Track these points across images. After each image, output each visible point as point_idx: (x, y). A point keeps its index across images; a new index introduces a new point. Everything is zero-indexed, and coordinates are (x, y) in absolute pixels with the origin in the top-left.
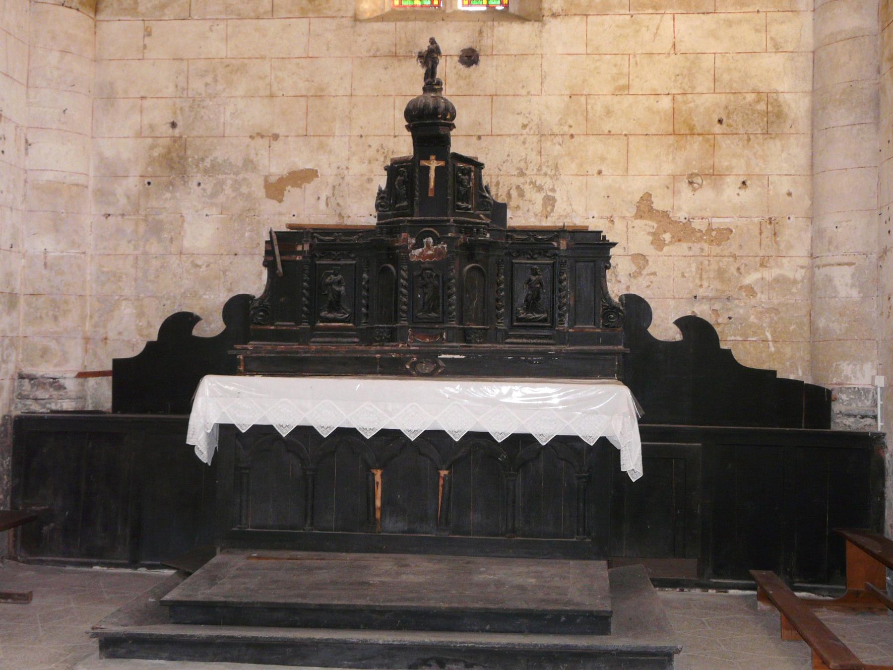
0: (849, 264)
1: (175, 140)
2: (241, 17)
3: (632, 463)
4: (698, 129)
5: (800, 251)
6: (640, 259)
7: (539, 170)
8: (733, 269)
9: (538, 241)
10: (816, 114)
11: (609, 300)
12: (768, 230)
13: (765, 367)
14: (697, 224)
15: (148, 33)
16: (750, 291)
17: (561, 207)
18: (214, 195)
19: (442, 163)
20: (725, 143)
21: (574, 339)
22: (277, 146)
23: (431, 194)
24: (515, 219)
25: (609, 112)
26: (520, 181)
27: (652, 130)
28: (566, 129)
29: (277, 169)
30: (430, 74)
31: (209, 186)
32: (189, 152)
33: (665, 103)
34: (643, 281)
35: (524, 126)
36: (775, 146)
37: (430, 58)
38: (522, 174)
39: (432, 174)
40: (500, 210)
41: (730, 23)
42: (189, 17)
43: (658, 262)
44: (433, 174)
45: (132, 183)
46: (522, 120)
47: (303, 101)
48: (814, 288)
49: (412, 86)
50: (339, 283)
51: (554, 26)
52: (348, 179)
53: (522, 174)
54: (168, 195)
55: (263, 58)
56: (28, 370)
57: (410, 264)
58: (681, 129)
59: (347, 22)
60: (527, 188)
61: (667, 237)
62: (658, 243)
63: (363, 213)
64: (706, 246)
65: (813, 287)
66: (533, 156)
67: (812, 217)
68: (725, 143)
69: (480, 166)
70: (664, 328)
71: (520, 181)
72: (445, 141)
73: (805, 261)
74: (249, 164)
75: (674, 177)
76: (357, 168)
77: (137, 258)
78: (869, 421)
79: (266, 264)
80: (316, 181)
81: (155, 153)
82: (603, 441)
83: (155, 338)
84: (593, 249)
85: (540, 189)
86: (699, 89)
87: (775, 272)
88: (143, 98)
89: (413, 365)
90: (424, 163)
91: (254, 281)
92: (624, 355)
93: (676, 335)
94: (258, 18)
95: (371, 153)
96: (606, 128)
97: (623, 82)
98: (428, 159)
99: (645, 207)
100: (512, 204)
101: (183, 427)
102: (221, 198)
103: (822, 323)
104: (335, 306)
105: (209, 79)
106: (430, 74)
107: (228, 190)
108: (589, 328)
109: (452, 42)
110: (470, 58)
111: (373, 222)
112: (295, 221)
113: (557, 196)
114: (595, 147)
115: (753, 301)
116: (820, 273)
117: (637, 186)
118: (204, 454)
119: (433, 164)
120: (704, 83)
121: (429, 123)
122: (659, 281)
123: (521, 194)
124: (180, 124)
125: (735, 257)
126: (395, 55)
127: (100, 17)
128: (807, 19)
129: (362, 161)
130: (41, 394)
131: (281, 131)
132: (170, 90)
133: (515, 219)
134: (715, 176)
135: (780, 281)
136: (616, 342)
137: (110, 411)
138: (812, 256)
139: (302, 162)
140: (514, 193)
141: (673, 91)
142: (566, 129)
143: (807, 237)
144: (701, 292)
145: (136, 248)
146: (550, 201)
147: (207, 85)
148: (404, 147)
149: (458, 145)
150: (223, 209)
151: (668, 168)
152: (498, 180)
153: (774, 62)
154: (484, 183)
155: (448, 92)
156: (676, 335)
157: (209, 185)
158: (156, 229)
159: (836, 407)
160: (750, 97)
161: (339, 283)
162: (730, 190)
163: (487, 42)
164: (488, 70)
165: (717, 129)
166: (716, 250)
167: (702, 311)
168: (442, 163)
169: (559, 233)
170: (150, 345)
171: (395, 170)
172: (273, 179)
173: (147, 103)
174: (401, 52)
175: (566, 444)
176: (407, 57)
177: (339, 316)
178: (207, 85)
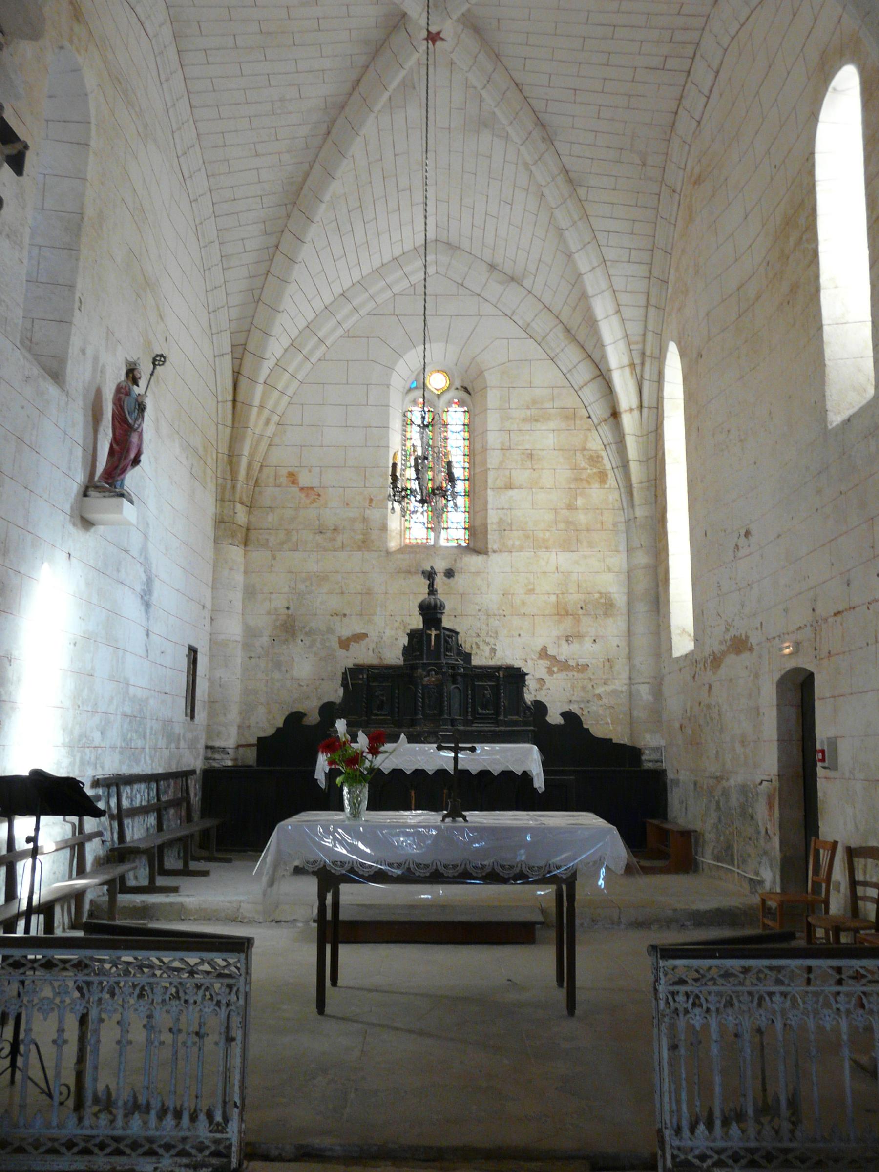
0: (648, 683)
1: (288, 616)
2: (325, 550)
3: (539, 783)
4: (570, 612)
5: (624, 676)
7: (487, 634)
8: (590, 686)
9: (490, 673)
10: (629, 604)
11: (525, 703)
12: (607, 665)
13: (608, 737)
14: (571, 663)
15: (274, 558)
16: (599, 697)
17: (499, 654)
18: (310, 647)
19: (438, 632)
20: (585, 620)
21: (507, 724)
22: (345, 620)
23: (432, 648)
24: (476, 661)
25: (523, 603)
26: (477, 640)
27: (547, 612)
28: (501, 612)
29: (346, 633)
30: (431, 586)
31: (307, 642)
32: (297, 624)
33: (553, 598)
34: (543, 693)
35: (479, 610)
36: (610, 621)
37: (430, 575)
38: (478, 636)
39: (433, 638)
40: (468, 657)
41: (585, 557)
42: (296, 550)
43: (550, 682)
44: (432, 640)
45: (265, 640)
46: (477, 608)
47: (359, 596)
49: (422, 593)
50: (383, 695)
51: (494, 557)
52: (385, 638)
53: (478, 636)
54: (285, 647)
55: (337, 572)
56: (211, 744)
57: (423, 685)
58: (562, 612)
59: (383, 554)
60: (481, 644)
61: (555, 669)
62: (550, 672)
63: (394, 656)
64: (575, 674)
65: (631, 695)
66: (484, 627)
67: (630, 658)
68: (585, 620)
69: (457, 633)
70: (554, 717)
71: (477, 640)
72: (440, 621)
73: (627, 681)
74: (330, 630)
75: (558, 638)
76: (389, 633)
77: (267, 682)
78: (659, 764)
79: (342, 685)
80: (367, 639)
81: (278, 623)
82: (525, 773)
83: (281, 725)
84: (515, 677)
85: (488, 644)
86: (571, 591)
87: (612, 687)
88: (271, 593)
89: (425, 738)
90: (429, 632)
92: (533, 731)
93: (560, 721)
94: (335, 551)
95: (396, 624)
96: (522, 612)
97: (531, 587)
98: (430, 630)
99: (543, 653)
100: (473, 652)
101: (313, 772)
102: (315, 649)
103: (635, 713)
104: (380, 708)
105: (308, 583)
106: (431, 586)
107: (318, 644)
108: (515, 718)
109: (440, 566)
110: (449, 574)
111: (402, 663)
112: (357, 661)
113: (497, 648)
114: (516, 621)
115: (601, 702)
116: (634, 687)
117: (538, 643)
119: (433, 633)
120: (573, 589)
121: (431, 612)
123: (478, 647)
124: (291, 608)
125: (591, 679)
126: (409, 572)
127: (247, 549)
128: (624, 555)
129: (392, 629)
130: (217, 756)
131: (347, 613)
132: (286, 589)
133: (476, 661)
134: (580, 636)
135: (614, 692)
136: (531, 723)
137: (255, 764)
138: (630, 678)
139: (359, 629)
140: (474, 646)
141: (557, 592)
142: (501, 612)
143: (627, 668)
144: (574, 698)
145: (267, 676)
146: (493, 651)
147: (306, 586)
148: (417, 622)
149: (446, 623)
150: (316, 654)
151: (555, 633)
152: (466, 641)
154: (460, 642)
155: (441, 596)
156: (560, 721)
157: (307, 642)
158: (278, 665)
159: (644, 758)
160: (597, 595)
161: (383, 695)
162: (588, 644)
163: (459, 565)
164: (459, 580)
165: (580, 612)
166: (581, 676)
167: (575, 708)
168: (438, 632)
169: (498, 668)
170: (279, 730)
172: (343, 638)
173: (273, 596)
174: (413, 570)
175: (507, 774)
176: (416, 573)
177: (383, 713)
178: (306, 586)
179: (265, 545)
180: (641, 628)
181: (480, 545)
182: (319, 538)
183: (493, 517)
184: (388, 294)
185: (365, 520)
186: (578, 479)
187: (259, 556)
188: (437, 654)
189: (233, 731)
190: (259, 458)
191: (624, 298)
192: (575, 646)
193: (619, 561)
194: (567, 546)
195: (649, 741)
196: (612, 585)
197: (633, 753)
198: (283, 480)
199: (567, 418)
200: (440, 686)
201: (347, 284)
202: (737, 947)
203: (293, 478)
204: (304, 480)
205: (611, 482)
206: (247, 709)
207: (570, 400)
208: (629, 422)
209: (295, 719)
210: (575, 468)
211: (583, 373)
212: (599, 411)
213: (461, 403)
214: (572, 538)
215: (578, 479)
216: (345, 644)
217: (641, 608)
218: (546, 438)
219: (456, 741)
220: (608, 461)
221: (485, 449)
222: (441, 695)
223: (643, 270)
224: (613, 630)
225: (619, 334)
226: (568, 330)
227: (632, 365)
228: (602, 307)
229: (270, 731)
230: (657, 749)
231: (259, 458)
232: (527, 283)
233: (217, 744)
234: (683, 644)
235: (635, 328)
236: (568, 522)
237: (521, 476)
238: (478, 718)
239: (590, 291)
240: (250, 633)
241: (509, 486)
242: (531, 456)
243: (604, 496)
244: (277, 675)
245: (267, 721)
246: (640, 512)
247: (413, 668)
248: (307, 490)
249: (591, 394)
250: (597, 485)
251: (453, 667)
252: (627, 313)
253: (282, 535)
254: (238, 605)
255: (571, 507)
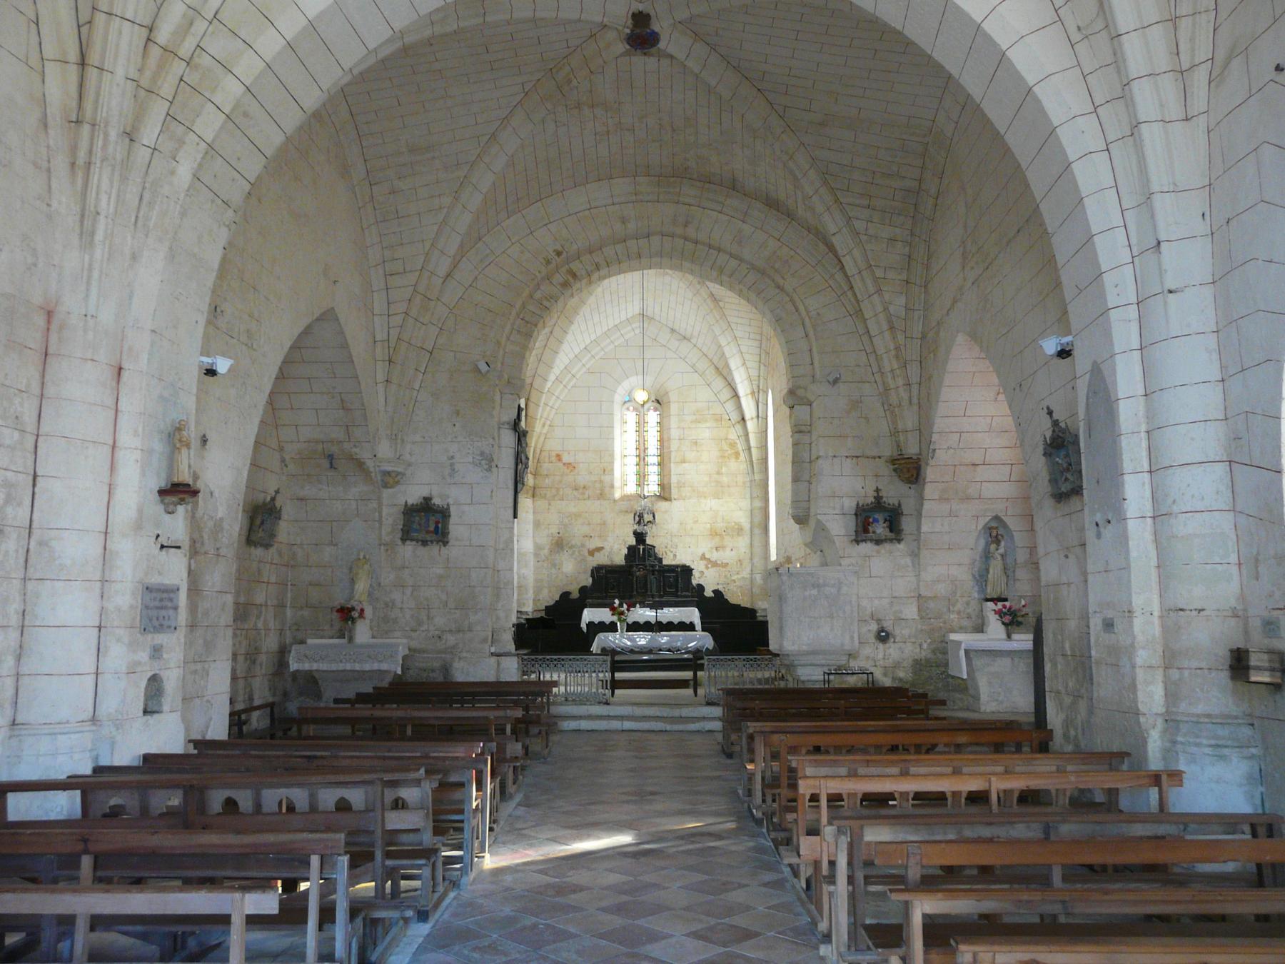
5: (748, 569)
6: (702, 572)
9: (672, 569)
24: (665, 562)
29: (592, 546)
44: (641, 551)
45: (546, 551)
48: (752, 580)
58: (714, 533)
70: (708, 593)
74: (583, 546)
76: (616, 546)
84: (687, 571)
91: (588, 581)
99: (703, 557)
118: (585, 629)
121: (640, 537)
122: (707, 579)
128: (749, 501)
133: (665, 562)
134: (723, 547)
136: (695, 596)
148: (633, 541)
149: (649, 541)
152: (660, 551)
153: (741, 513)
158: (554, 565)
169: (677, 566)
171: (630, 548)
179: (545, 497)
180: (757, 543)
181: (667, 495)
182: (575, 493)
183: (674, 479)
184: (612, 346)
185: (601, 481)
186: (723, 457)
187: (541, 503)
188: (644, 559)
189: (531, 602)
190: (539, 446)
191: (747, 357)
192: (721, 553)
193: (746, 504)
194: (717, 496)
195: (761, 605)
196: (743, 518)
197: (752, 612)
198: (553, 459)
199: (717, 420)
200: (645, 577)
201: (588, 341)
202: (1208, 837)
203: (559, 457)
204: (566, 458)
205: (742, 458)
206: (538, 590)
207: (718, 410)
208: (751, 425)
209: (565, 595)
210: (721, 450)
211: (726, 394)
212: (735, 417)
213: (656, 410)
214: (719, 491)
215: (723, 457)
216: (591, 553)
217: (757, 531)
218: (705, 433)
219: (656, 606)
220: (740, 446)
221: (669, 439)
222: (646, 584)
223: (757, 343)
224: (742, 543)
225: (744, 376)
226: (717, 368)
227: (753, 393)
228: (734, 363)
229: (552, 603)
230: (765, 610)
231: (539, 446)
232: (694, 341)
233: (523, 610)
234: (773, 557)
235: (754, 373)
236: (717, 482)
237: (690, 455)
238: (666, 593)
239: (727, 355)
240: (538, 548)
241: (684, 462)
242: (696, 443)
243: (738, 466)
244: (553, 571)
245: (549, 597)
246: (757, 477)
247: (631, 567)
248: (568, 465)
249: (730, 406)
250: (733, 460)
251: (653, 566)
252: (749, 364)
253: (554, 491)
254: (531, 531)
255: (718, 473)
